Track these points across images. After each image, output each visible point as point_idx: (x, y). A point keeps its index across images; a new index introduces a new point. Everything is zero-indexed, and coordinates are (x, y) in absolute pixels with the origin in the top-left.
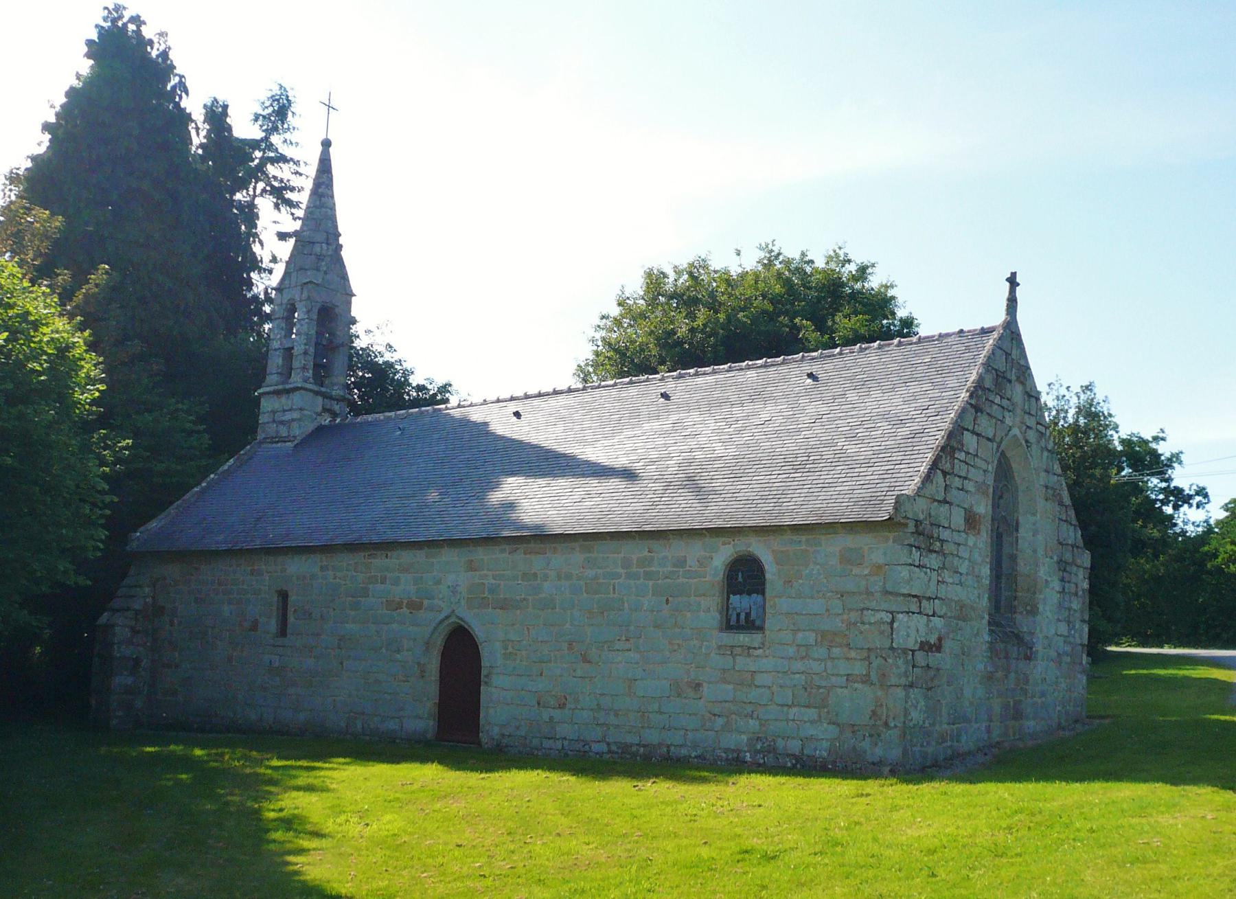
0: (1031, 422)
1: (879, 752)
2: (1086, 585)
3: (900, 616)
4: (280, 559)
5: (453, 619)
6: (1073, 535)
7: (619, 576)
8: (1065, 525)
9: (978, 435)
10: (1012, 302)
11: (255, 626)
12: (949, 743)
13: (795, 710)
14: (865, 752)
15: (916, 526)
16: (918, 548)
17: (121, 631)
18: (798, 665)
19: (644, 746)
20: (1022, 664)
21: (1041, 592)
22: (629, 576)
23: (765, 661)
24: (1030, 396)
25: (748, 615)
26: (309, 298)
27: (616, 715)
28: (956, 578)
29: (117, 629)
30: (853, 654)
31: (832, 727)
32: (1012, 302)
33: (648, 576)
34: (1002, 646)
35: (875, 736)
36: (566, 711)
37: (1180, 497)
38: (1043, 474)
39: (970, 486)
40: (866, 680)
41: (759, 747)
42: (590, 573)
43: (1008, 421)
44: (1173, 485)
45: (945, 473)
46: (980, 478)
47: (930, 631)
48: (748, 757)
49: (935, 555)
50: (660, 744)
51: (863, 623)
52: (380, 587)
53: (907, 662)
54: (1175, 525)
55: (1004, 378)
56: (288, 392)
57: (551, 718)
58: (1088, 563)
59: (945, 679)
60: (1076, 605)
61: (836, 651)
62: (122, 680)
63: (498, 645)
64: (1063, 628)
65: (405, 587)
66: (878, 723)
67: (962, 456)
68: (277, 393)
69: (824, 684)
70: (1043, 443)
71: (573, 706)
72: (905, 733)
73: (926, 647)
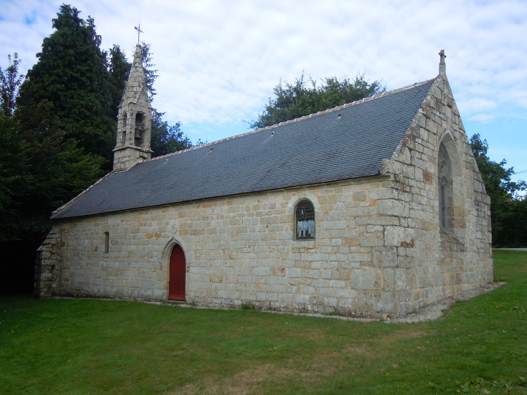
0: (457, 128)
1: (380, 305)
2: (489, 214)
3: (388, 227)
4: (106, 218)
5: (174, 241)
6: (481, 187)
7: (244, 215)
8: (477, 182)
9: (428, 131)
10: (442, 65)
11: (96, 250)
12: (421, 299)
13: (333, 281)
14: (372, 305)
15: (395, 177)
16: (397, 189)
17: (45, 254)
18: (333, 257)
19: (258, 301)
20: (459, 254)
21: (467, 216)
22: (250, 215)
23: (316, 255)
24: (455, 114)
25: (307, 232)
26: (131, 110)
27: (245, 286)
28: (420, 207)
29: (43, 253)
30: (362, 250)
31: (353, 291)
32: (442, 65)
33: (258, 214)
34: (448, 244)
35: (378, 296)
36: (222, 284)
37: (514, 186)
38: (464, 155)
39: (425, 157)
40: (371, 264)
41: (315, 302)
42: (232, 215)
43: (444, 125)
44: (510, 182)
45: (410, 150)
46: (430, 154)
47: (407, 236)
48: (310, 308)
49: (406, 194)
50: (266, 300)
51: (368, 232)
52: (144, 228)
53: (394, 253)
54: (512, 198)
55: (441, 103)
56: (124, 149)
57: (216, 287)
58: (489, 202)
59: (417, 263)
60: (485, 223)
61: (353, 248)
62: (45, 275)
63: (193, 252)
64: (479, 235)
65: (154, 227)
66: (379, 288)
67: (420, 141)
68: (120, 150)
69: (347, 267)
70: (463, 139)
71: (225, 282)
72: (394, 295)
73: (405, 245)
